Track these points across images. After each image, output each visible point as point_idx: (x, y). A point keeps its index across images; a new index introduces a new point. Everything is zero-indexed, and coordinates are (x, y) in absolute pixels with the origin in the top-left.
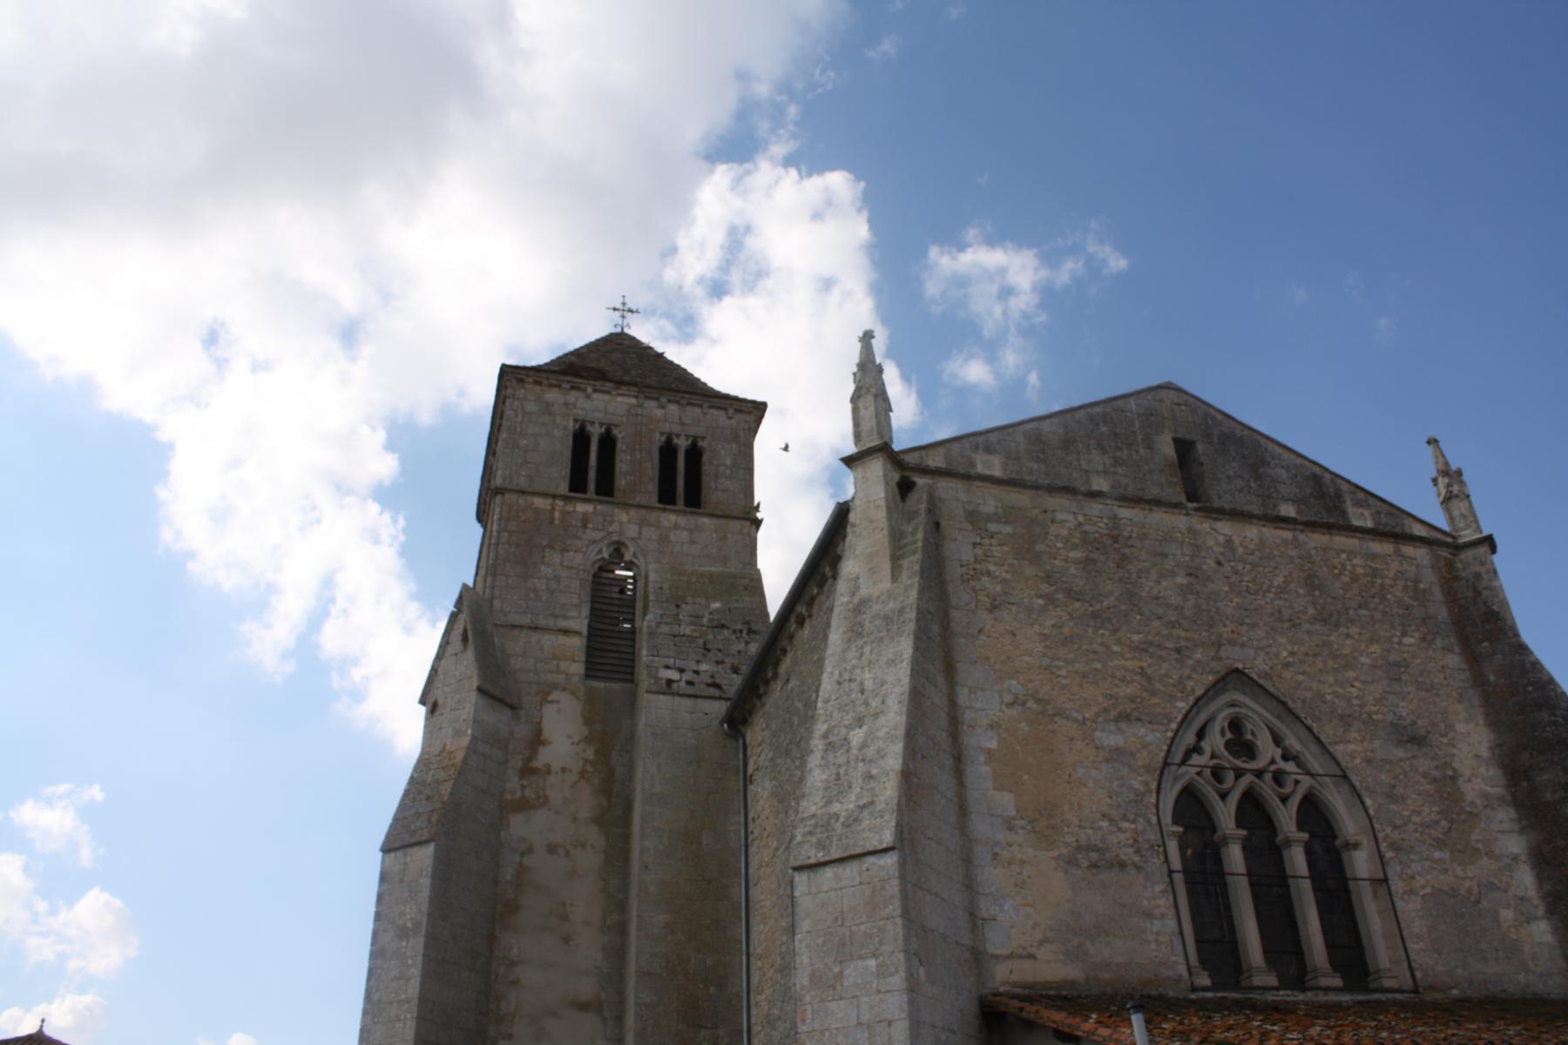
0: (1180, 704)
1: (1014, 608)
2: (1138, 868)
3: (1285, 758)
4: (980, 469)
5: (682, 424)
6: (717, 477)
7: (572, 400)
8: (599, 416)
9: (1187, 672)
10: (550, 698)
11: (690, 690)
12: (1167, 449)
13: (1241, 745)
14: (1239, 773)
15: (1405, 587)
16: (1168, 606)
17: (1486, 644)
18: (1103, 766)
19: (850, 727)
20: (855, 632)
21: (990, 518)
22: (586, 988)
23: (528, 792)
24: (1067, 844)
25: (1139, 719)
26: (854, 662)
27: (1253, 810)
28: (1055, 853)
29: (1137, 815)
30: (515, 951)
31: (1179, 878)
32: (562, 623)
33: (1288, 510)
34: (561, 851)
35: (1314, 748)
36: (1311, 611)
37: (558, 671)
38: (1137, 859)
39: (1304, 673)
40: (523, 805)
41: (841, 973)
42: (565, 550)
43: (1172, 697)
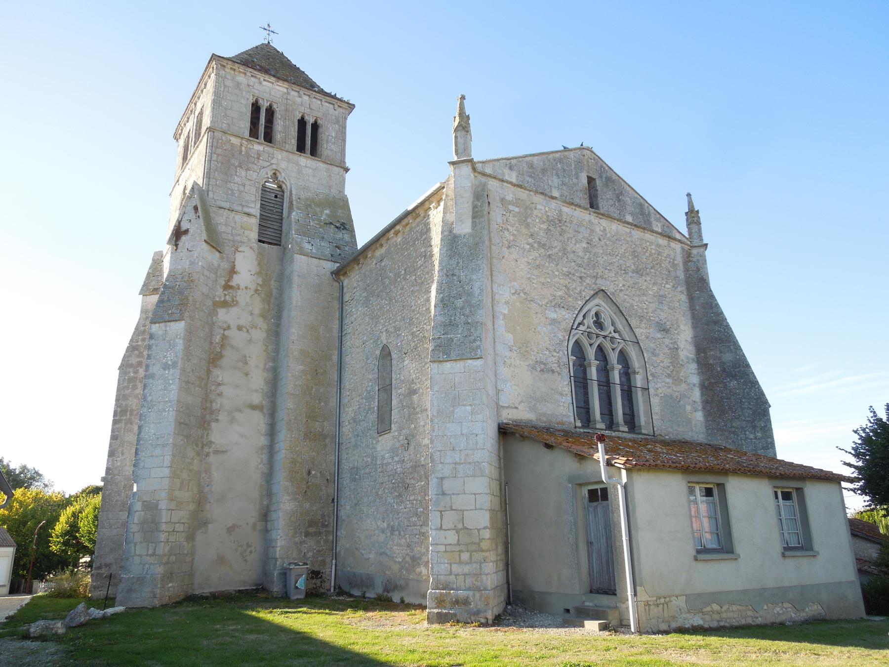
0: (580, 303)
2: (559, 374)
3: (615, 332)
4: (507, 178)
7: (252, 84)
8: (266, 96)
12: (585, 181)
13: (599, 324)
14: (598, 336)
16: (579, 256)
18: (548, 327)
21: (510, 203)
22: (256, 399)
32: (246, 210)
33: (629, 219)
34: (244, 329)
35: (627, 328)
40: (225, 304)
43: (577, 299)
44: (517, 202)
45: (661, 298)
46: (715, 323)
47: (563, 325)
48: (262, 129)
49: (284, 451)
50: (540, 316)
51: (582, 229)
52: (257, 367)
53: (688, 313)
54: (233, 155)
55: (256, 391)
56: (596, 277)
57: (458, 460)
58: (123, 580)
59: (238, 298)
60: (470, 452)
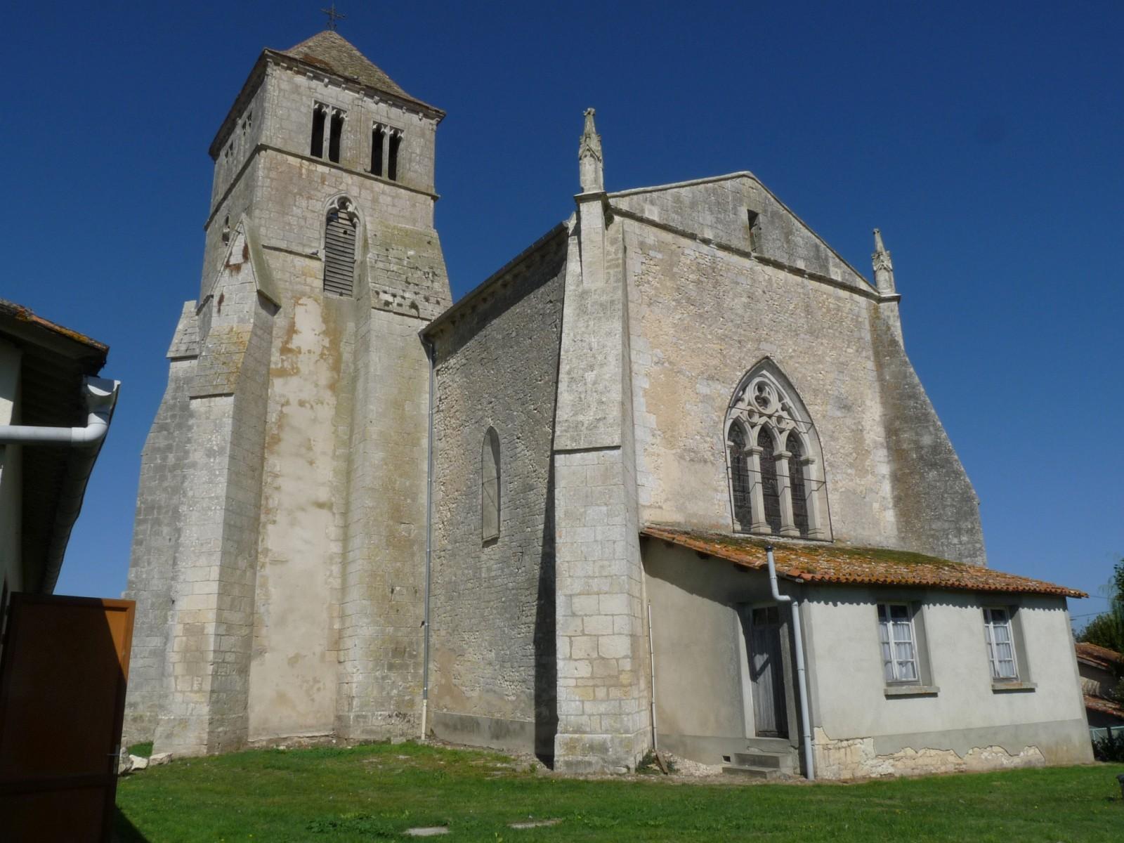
0: (739, 373)
1: (660, 305)
2: (713, 464)
3: (783, 410)
4: (647, 215)
5: (388, 118)
6: (410, 161)
7: (314, 86)
9: (743, 355)
10: (300, 302)
11: (400, 310)
15: (852, 319)
17: (888, 358)
18: (700, 405)
19: (584, 370)
20: (582, 311)
21: (652, 248)
22: (323, 495)
23: (286, 364)
24: (679, 447)
25: (718, 380)
26: (583, 329)
27: (766, 436)
28: (674, 451)
29: (714, 434)
30: (278, 468)
31: (730, 469)
33: (801, 265)
35: (798, 405)
36: (805, 326)
37: (305, 284)
38: (712, 458)
39: (798, 363)
40: (282, 373)
41: (585, 512)
42: (309, 198)
44: (660, 247)
45: (842, 367)
46: (910, 397)
47: (718, 402)
48: (326, 145)
49: (360, 562)
50: (689, 391)
51: (742, 279)
52: (324, 453)
53: (877, 385)
54: (291, 179)
55: (323, 484)
56: (759, 341)
57: (590, 573)
58: (162, 723)
59: (299, 365)
60: (606, 563)
